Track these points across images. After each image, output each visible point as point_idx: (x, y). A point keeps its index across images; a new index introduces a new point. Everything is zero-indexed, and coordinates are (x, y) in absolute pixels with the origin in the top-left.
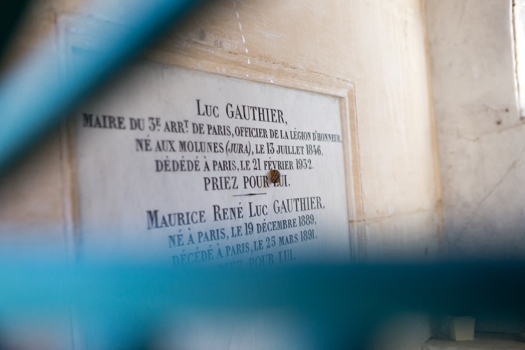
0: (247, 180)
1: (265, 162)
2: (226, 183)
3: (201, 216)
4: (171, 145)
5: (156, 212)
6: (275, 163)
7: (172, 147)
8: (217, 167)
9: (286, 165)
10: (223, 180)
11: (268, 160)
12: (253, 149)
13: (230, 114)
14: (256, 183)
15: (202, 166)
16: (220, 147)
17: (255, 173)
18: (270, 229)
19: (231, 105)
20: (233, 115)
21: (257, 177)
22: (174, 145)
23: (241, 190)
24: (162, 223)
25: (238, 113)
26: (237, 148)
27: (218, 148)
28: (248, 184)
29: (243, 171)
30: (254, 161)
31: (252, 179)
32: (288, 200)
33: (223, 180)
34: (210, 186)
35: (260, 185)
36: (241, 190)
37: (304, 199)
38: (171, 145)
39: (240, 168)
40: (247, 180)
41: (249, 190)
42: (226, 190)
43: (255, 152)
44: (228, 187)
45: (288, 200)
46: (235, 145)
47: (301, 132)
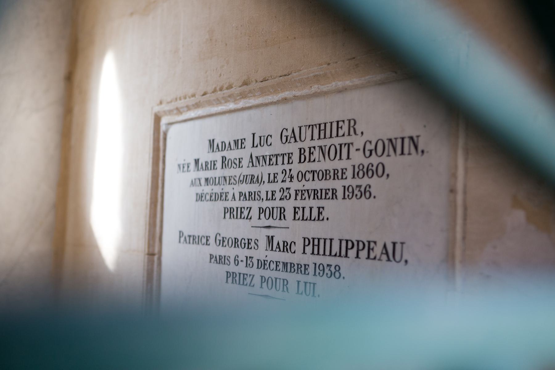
0: (261, 211)
1: (296, 191)
2: (241, 212)
3: (207, 240)
4: (200, 181)
5: (272, 237)
6: (310, 192)
7: (200, 183)
8: (242, 198)
9: (326, 194)
12: (266, 179)
13: (284, 139)
14: (271, 214)
15: (230, 196)
16: (234, 179)
17: (270, 204)
18: (271, 269)
19: (287, 130)
23: (255, 221)
24: (382, 253)
25: (293, 136)
26: (249, 179)
27: (232, 180)
28: (262, 216)
29: (268, 202)
30: (282, 190)
31: (268, 210)
32: (394, 244)
33: (239, 210)
34: (230, 280)
35: (275, 217)
36: (255, 221)
37: (319, 240)
38: (200, 181)
39: (265, 199)
40: (261, 211)
41: (265, 222)
44: (243, 217)
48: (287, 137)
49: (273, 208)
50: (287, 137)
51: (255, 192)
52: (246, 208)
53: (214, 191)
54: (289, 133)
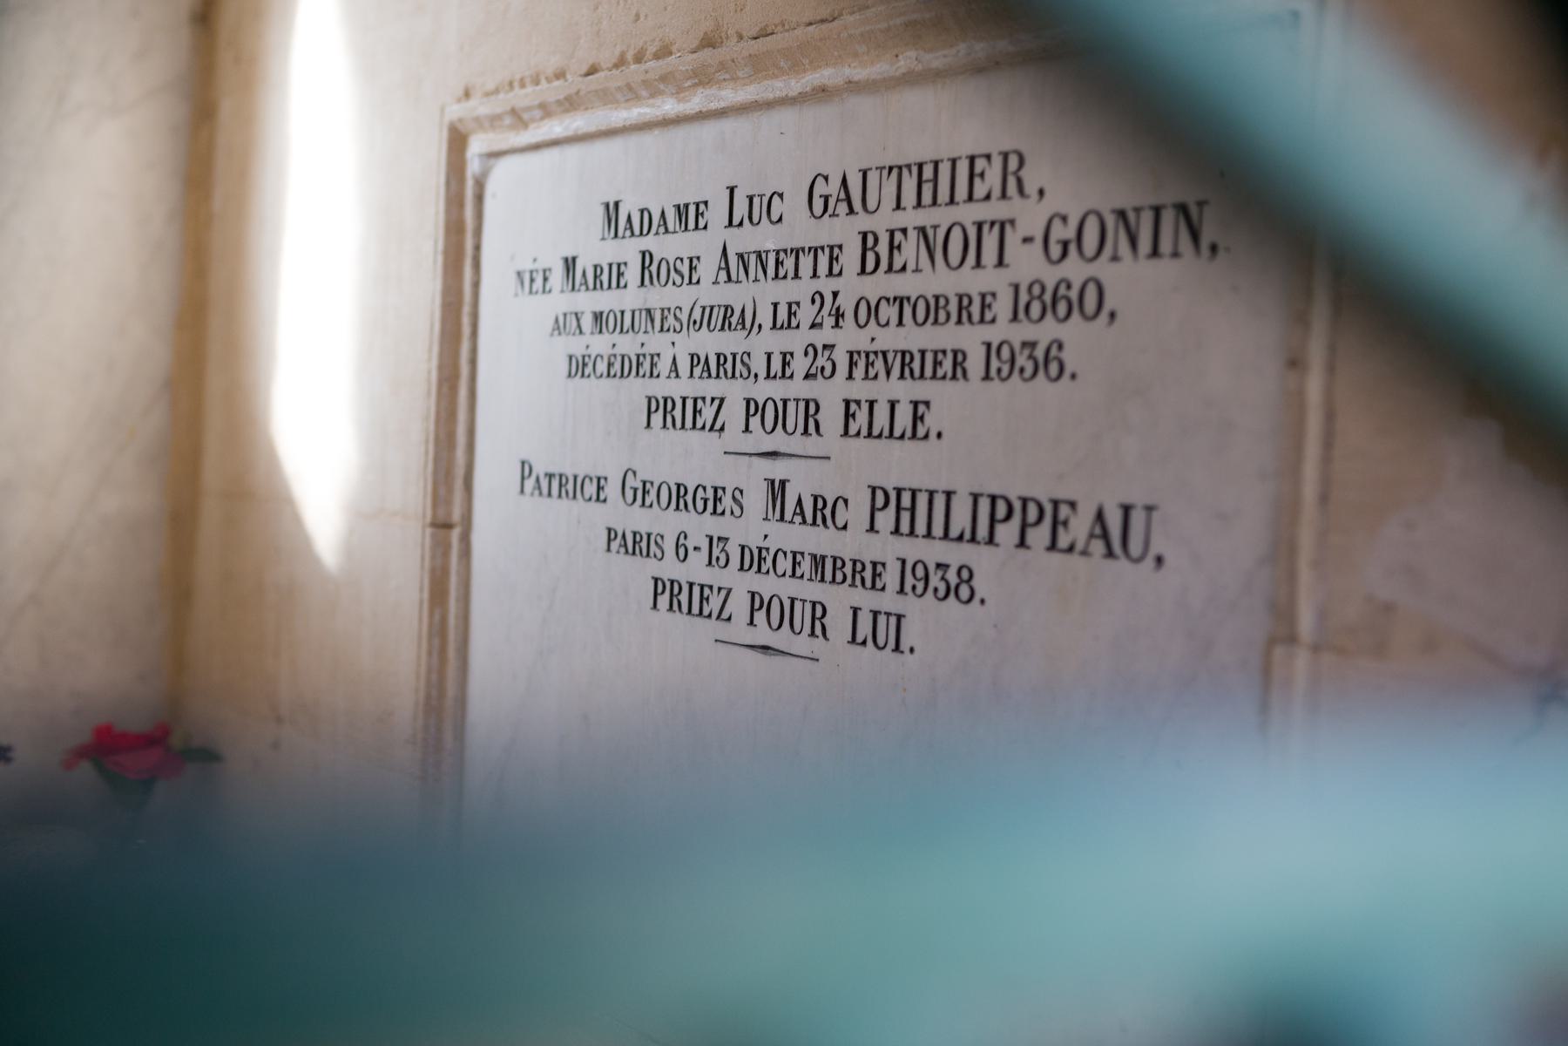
1: (851, 354)
2: (696, 411)
3: (599, 488)
5: (783, 483)
6: (890, 357)
7: (579, 326)
9: (937, 364)
10: (690, 404)
11: (864, 345)
12: (765, 317)
14: (780, 419)
15: (664, 366)
17: (777, 390)
19: (826, 178)
20: (825, 210)
21: (785, 402)
22: (583, 322)
23: (734, 436)
25: (842, 195)
26: (718, 315)
27: (671, 321)
29: (771, 382)
30: (812, 350)
34: (657, 419)
35: (790, 428)
36: (734, 436)
39: (762, 374)
40: (753, 408)
42: (696, 433)
43: (768, 323)
45: (1127, 510)
46: (712, 308)
47: (685, 256)
48: (826, 199)
49: (785, 402)
50: (826, 199)
51: (734, 356)
52: (708, 401)
53: (618, 351)
54: (834, 188)
